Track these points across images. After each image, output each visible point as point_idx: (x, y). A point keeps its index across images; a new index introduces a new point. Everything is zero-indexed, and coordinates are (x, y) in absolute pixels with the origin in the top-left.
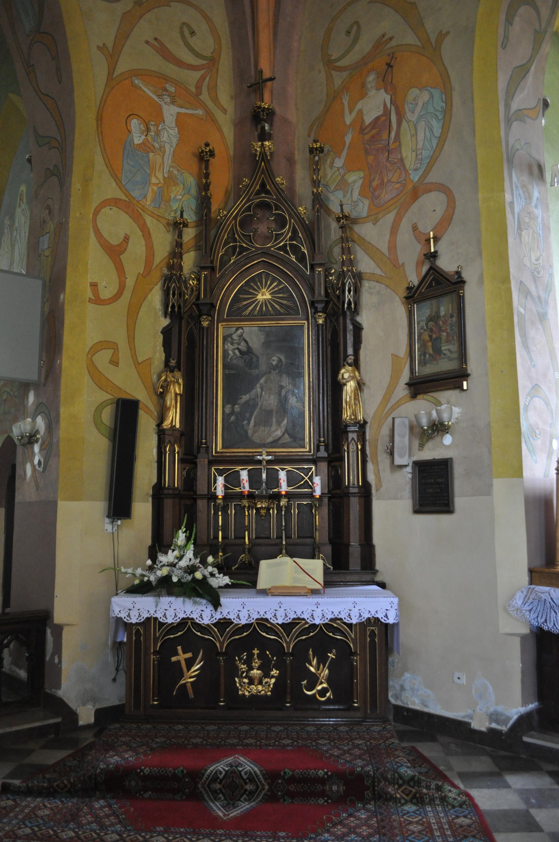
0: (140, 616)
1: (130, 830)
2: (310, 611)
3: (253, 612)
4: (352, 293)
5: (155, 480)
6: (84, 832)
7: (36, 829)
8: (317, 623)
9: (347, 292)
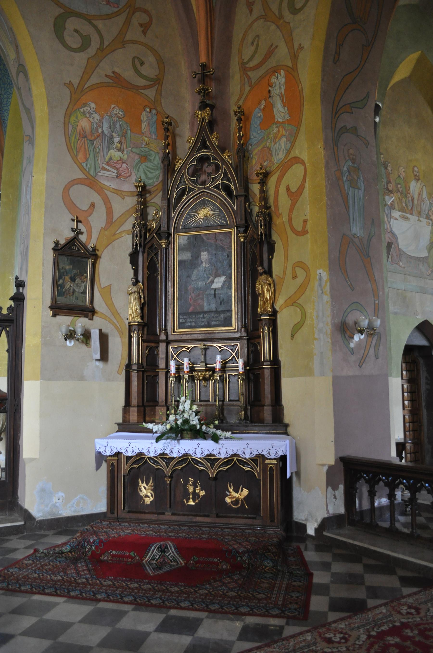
0: (112, 451)
1: (93, 578)
2: (147, 448)
3: (205, 449)
4: (267, 228)
5: (127, 362)
6: (67, 578)
7: (41, 575)
8: (175, 456)
9: (260, 228)
